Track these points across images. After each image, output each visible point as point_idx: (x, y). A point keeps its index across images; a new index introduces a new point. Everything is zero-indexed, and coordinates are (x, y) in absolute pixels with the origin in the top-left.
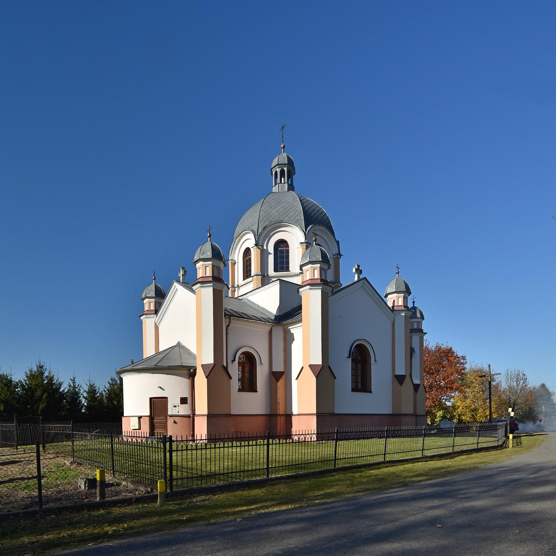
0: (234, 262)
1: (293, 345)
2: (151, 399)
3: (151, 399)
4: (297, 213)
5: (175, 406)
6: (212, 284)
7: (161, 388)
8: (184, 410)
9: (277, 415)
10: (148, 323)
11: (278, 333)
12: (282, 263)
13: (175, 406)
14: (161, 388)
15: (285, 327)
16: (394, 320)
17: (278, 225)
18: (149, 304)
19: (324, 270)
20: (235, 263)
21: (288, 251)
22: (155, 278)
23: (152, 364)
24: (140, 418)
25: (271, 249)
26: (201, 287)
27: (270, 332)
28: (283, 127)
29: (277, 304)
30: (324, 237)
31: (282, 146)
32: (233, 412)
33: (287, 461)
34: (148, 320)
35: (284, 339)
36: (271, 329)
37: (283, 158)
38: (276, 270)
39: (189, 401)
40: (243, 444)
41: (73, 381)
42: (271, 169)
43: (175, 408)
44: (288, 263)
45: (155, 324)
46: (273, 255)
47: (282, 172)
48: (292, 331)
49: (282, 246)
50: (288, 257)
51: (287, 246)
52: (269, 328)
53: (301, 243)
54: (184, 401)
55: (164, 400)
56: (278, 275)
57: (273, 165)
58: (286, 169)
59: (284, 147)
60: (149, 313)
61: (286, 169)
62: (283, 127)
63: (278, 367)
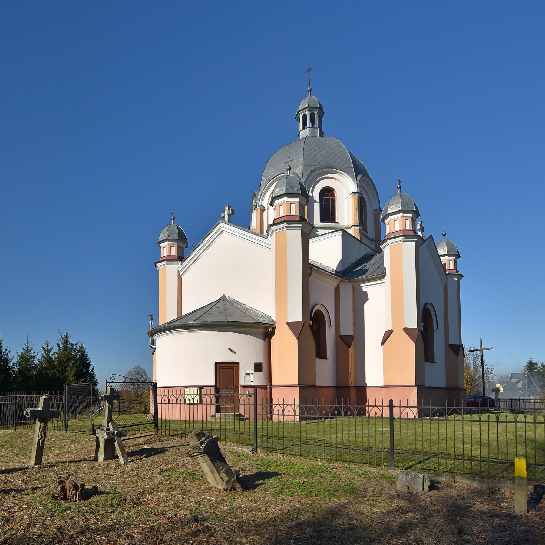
0: (262, 208)
1: (365, 305)
2: (216, 363)
3: (216, 363)
4: (345, 160)
5: (248, 374)
6: (301, 225)
7: (231, 350)
8: (257, 379)
9: (348, 387)
10: (168, 272)
11: (346, 290)
12: (328, 213)
13: (248, 374)
14: (231, 350)
15: (355, 284)
16: (446, 285)
17: (316, 172)
18: (168, 248)
19: (181, 248)
20: (264, 210)
21: (333, 201)
22: (174, 218)
23: (189, 322)
24: (201, 388)
25: (316, 196)
26: (287, 227)
27: (337, 290)
28: (309, 69)
29: (339, 258)
30: (367, 189)
31: (309, 89)
32: (318, 384)
33: (467, 438)
34: (168, 267)
35: (353, 298)
36: (338, 285)
37: (315, 100)
38: (322, 221)
39: (264, 367)
40: (484, 417)
41: (66, 341)
42: (298, 112)
43: (248, 377)
44: (334, 213)
45: (179, 273)
46: (319, 204)
47: (312, 116)
48: (364, 289)
49: (328, 194)
50: (334, 207)
51: (333, 195)
52: (336, 284)
53: (354, 192)
54: (258, 367)
55: (235, 365)
56: (325, 226)
57: (301, 108)
58: (316, 113)
59: (310, 90)
60: (169, 258)
61: (316, 113)
62: (309, 69)
63: (347, 330)
